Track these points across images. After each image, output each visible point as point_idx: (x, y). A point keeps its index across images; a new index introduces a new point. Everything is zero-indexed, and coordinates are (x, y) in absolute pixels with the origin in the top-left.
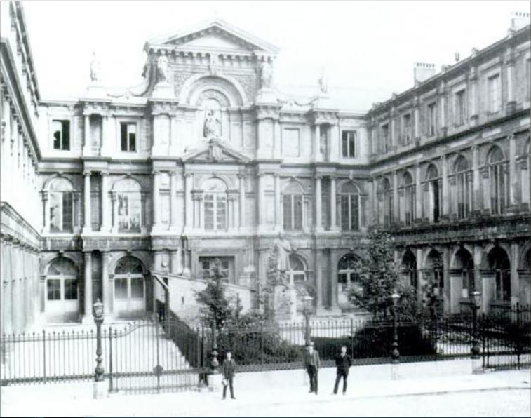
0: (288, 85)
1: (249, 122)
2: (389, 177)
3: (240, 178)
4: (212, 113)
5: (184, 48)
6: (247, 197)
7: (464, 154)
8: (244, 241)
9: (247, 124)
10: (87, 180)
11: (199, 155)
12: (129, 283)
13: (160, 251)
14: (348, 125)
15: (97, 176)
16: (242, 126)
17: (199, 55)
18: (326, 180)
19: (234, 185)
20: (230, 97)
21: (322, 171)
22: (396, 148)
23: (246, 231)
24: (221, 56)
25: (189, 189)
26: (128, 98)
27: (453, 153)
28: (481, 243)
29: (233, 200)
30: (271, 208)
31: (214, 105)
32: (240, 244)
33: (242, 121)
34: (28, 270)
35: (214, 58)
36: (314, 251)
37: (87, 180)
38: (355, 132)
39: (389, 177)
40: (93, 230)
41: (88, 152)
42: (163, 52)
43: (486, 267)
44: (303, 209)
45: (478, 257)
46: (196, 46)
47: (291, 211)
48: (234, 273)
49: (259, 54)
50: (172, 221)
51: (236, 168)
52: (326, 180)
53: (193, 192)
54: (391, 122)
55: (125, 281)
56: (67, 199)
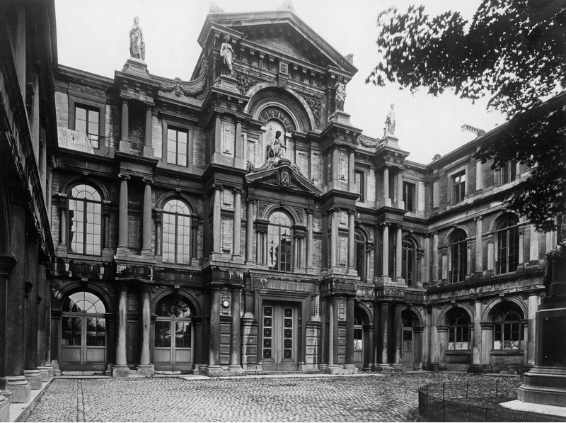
1: (317, 152)
3: (308, 213)
4: (278, 134)
6: (315, 238)
8: (311, 285)
9: (315, 154)
10: (124, 186)
11: (266, 178)
13: (221, 286)
14: (409, 176)
15: (137, 186)
16: (309, 157)
18: (393, 229)
19: (301, 221)
21: (391, 217)
22: (481, 191)
23: (315, 271)
25: (253, 218)
26: (178, 95)
28: (484, 299)
29: (300, 239)
30: (342, 249)
31: (276, 127)
32: (307, 288)
33: (309, 151)
35: (284, 66)
36: (377, 304)
38: (414, 185)
43: (486, 319)
45: (479, 312)
48: (300, 322)
51: (302, 201)
52: (393, 229)
53: (256, 222)
56: (402, 329)
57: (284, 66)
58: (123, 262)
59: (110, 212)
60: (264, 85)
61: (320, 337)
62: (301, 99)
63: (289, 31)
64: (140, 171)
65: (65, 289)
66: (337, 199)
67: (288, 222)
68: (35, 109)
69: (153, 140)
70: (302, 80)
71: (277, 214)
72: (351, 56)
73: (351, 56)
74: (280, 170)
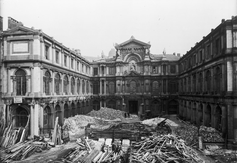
0: (156, 51)
2: (201, 72)
5: (125, 48)
7: (209, 69)
10: (101, 82)
12: (96, 106)
17: (129, 49)
20: (136, 58)
24: (134, 49)
27: (206, 69)
31: (133, 62)
34: (7, 114)
35: (133, 49)
37: (101, 82)
39: (201, 72)
40: (46, 95)
41: (101, 75)
42: (119, 49)
44: (228, 66)
46: (127, 47)
47: (212, 51)
49: (145, 47)
50: (8, 90)
51: (138, 78)
52: (103, 81)
54: (210, 44)
55: (95, 106)
57: (133, 49)
58: (101, 96)
59: (145, 89)
60: (129, 54)
61: (142, 108)
62: (138, 54)
63: (133, 42)
64: (103, 79)
65: (29, 79)
66: (117, 78)
67: (135, 83)
68: (92, 70)
69: (182, 56)
70: (138, 50)
71: (132, 81)
72: (149, 42)
73: (149, 42)
74: (131, 73)
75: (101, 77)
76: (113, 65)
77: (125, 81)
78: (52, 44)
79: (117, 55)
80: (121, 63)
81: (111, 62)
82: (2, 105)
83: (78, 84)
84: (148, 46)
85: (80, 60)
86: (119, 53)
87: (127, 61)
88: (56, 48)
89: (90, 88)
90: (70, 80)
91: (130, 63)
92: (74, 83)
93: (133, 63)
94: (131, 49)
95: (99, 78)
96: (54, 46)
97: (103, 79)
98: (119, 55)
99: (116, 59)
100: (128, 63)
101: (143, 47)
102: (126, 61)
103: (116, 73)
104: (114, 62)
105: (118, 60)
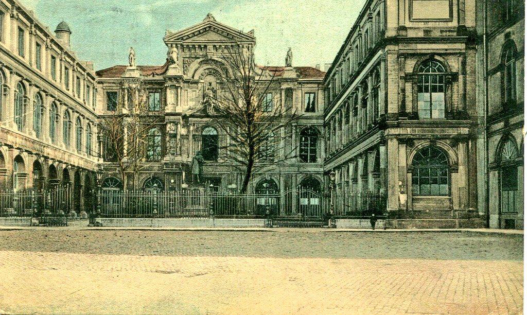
0: (266, 55)
31: (211, 79)
35: (210, 47)
41: (125, 111)
46: (201, 39)
72: (252, 32)
75: (127, 116)
76: (158, 84)
77: (188, 127)
78: (13, 9)
79: (170, 61)
80: (177, 78)
81: (154, 78)
82: (484, 96)
83: (65, 123)
84: (251, 39)
85: (83, 73)
86: (174, 56)
87: (196, 78)
88: (18, 19)
89: (95, 147)
90: (74, 121)
91: (202, 81)
92: (57, 118)
93: (210, 84)
94: (205, 46)
95: (122, 116)
96: (15, 12)
97: (129, 120)
98: (175, 60)
99: (167, 70)
100: (197, 83)
101: (237, 41)
102: (193, 77)
103: (166, 105)
104: (161, 78)
105: (171, 72)
